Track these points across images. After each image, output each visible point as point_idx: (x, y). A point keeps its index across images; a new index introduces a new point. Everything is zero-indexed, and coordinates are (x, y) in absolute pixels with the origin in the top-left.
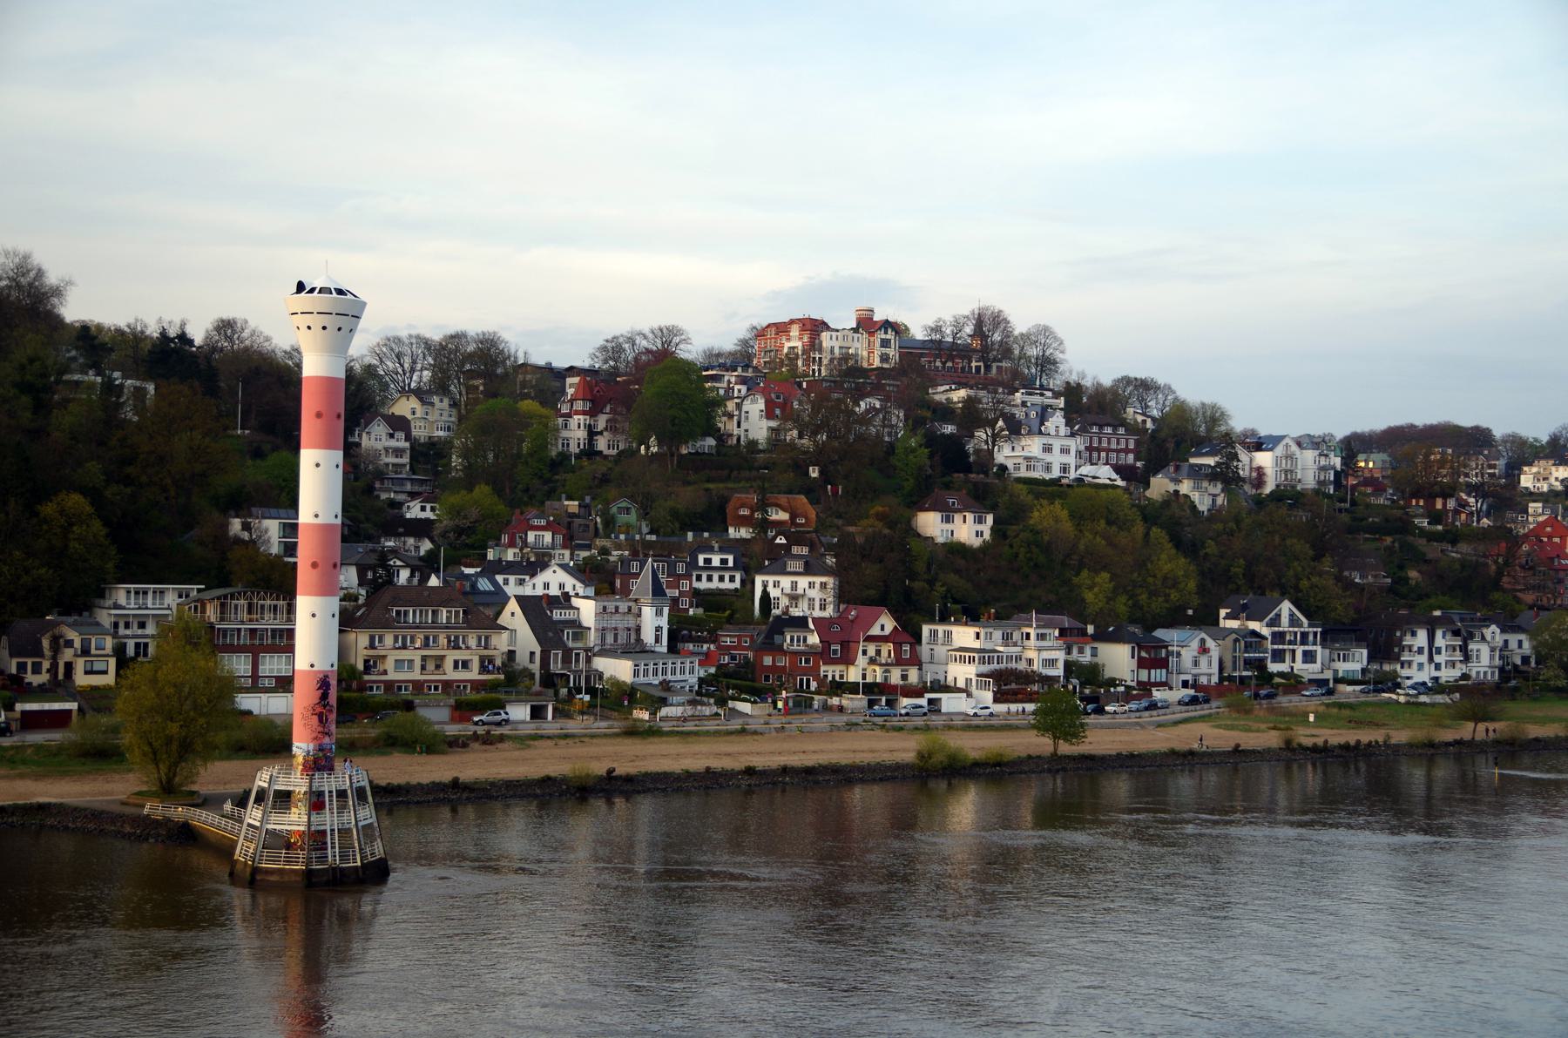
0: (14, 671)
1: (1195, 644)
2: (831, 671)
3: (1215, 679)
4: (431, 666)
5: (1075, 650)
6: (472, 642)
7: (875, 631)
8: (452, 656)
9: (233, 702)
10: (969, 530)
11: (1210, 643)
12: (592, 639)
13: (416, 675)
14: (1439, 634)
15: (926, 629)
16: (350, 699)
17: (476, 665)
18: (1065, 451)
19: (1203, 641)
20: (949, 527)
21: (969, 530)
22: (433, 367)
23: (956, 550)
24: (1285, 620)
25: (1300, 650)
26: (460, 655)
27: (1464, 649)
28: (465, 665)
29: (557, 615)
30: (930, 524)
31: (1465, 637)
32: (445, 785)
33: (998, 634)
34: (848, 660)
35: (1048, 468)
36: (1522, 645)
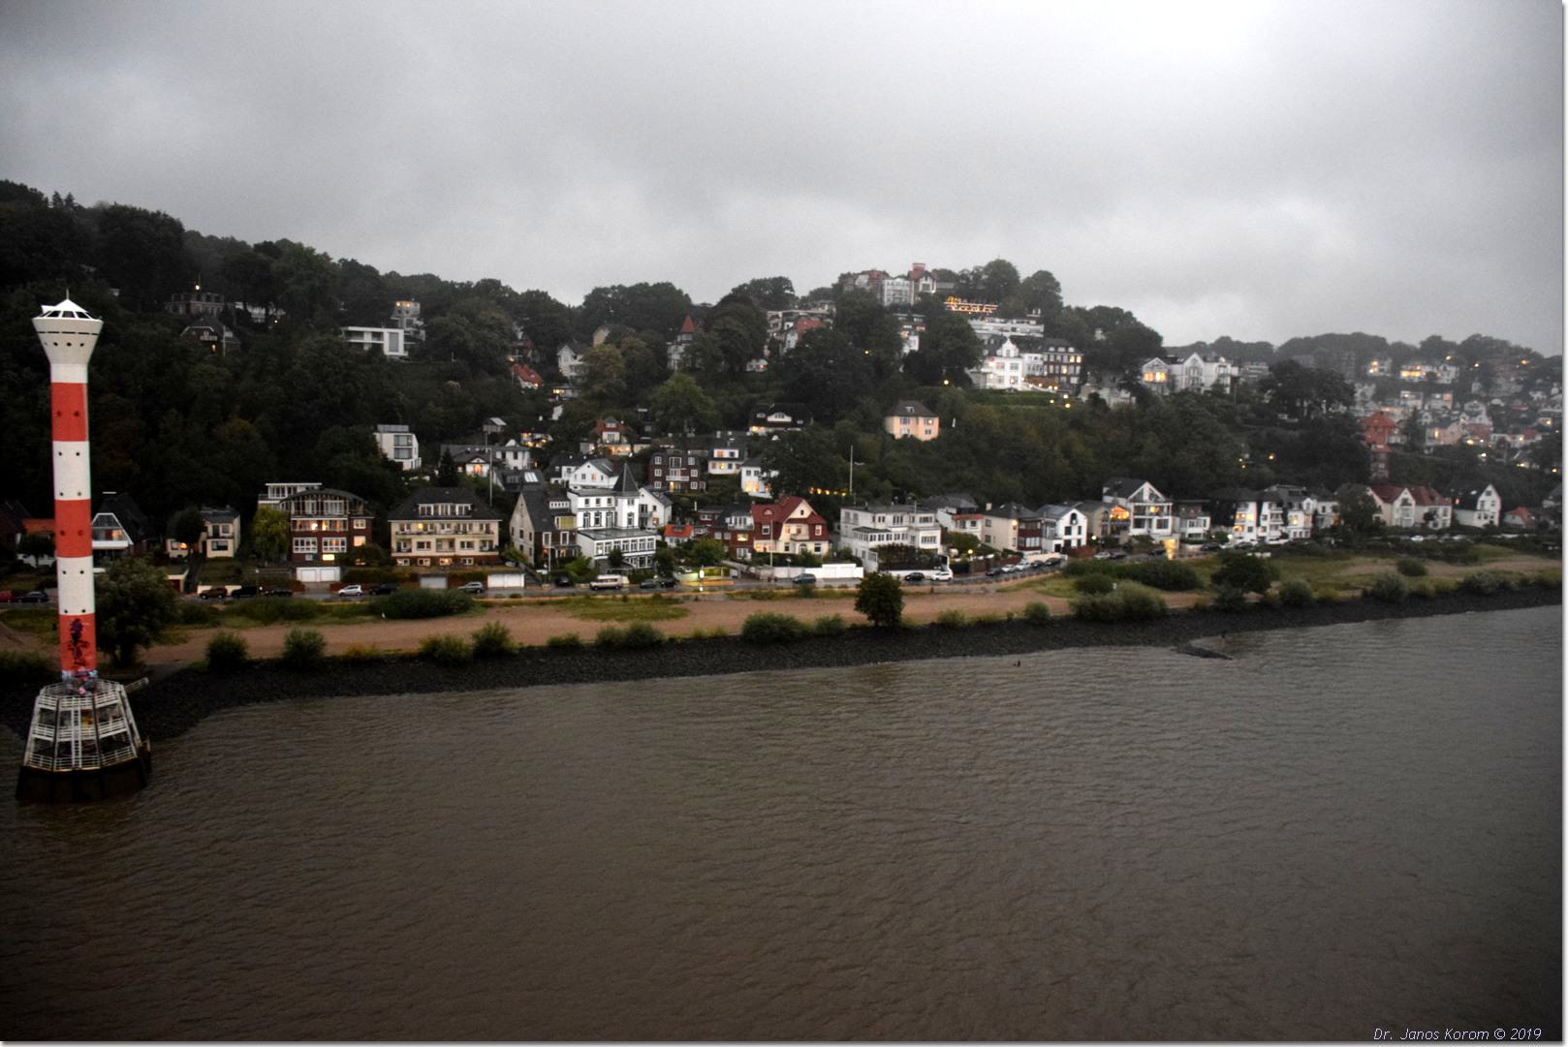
1: (1066, 518)
2: (759, 546)
3: (1084, 543)
4: (446, 546)
5: (968, 524)
6: (476, 528)
7: (796, 514)
8: (459, 539)
9: (294, 571)
10: (926, 429)
11: (1081, 517)
12: (579, 523)
13: (433, 552)
14: (1265, 506)
15: (843, 512)
16: (127, 614)
17: (477, 544)
18: (1014, 367)
19: (1074, 516)
21: (926, 429)
23: (909, 441)
24: (1146, 497)
25: (1155, 519)
26: (465, 539)
27: (1285, 517)
28: (421, 545)
29: (554, 505)
30: (898, 427)
31: (1284, 507)
35: (1001, 380)
36: (1328, 511)
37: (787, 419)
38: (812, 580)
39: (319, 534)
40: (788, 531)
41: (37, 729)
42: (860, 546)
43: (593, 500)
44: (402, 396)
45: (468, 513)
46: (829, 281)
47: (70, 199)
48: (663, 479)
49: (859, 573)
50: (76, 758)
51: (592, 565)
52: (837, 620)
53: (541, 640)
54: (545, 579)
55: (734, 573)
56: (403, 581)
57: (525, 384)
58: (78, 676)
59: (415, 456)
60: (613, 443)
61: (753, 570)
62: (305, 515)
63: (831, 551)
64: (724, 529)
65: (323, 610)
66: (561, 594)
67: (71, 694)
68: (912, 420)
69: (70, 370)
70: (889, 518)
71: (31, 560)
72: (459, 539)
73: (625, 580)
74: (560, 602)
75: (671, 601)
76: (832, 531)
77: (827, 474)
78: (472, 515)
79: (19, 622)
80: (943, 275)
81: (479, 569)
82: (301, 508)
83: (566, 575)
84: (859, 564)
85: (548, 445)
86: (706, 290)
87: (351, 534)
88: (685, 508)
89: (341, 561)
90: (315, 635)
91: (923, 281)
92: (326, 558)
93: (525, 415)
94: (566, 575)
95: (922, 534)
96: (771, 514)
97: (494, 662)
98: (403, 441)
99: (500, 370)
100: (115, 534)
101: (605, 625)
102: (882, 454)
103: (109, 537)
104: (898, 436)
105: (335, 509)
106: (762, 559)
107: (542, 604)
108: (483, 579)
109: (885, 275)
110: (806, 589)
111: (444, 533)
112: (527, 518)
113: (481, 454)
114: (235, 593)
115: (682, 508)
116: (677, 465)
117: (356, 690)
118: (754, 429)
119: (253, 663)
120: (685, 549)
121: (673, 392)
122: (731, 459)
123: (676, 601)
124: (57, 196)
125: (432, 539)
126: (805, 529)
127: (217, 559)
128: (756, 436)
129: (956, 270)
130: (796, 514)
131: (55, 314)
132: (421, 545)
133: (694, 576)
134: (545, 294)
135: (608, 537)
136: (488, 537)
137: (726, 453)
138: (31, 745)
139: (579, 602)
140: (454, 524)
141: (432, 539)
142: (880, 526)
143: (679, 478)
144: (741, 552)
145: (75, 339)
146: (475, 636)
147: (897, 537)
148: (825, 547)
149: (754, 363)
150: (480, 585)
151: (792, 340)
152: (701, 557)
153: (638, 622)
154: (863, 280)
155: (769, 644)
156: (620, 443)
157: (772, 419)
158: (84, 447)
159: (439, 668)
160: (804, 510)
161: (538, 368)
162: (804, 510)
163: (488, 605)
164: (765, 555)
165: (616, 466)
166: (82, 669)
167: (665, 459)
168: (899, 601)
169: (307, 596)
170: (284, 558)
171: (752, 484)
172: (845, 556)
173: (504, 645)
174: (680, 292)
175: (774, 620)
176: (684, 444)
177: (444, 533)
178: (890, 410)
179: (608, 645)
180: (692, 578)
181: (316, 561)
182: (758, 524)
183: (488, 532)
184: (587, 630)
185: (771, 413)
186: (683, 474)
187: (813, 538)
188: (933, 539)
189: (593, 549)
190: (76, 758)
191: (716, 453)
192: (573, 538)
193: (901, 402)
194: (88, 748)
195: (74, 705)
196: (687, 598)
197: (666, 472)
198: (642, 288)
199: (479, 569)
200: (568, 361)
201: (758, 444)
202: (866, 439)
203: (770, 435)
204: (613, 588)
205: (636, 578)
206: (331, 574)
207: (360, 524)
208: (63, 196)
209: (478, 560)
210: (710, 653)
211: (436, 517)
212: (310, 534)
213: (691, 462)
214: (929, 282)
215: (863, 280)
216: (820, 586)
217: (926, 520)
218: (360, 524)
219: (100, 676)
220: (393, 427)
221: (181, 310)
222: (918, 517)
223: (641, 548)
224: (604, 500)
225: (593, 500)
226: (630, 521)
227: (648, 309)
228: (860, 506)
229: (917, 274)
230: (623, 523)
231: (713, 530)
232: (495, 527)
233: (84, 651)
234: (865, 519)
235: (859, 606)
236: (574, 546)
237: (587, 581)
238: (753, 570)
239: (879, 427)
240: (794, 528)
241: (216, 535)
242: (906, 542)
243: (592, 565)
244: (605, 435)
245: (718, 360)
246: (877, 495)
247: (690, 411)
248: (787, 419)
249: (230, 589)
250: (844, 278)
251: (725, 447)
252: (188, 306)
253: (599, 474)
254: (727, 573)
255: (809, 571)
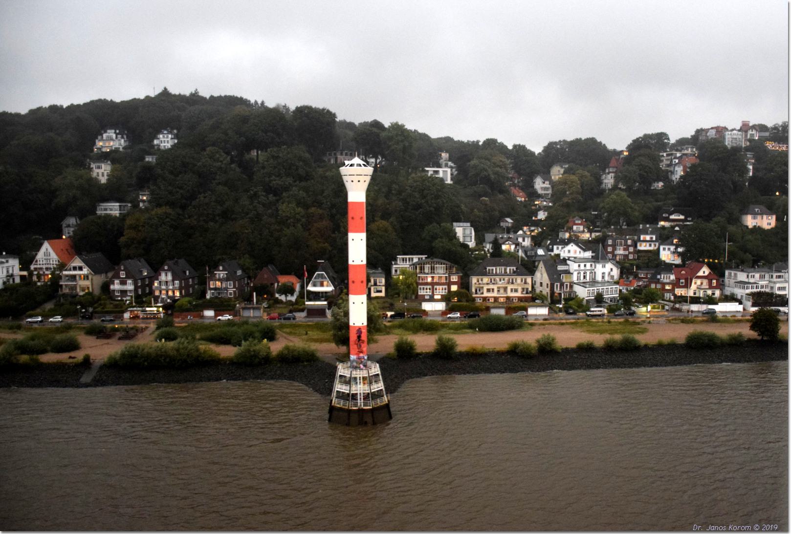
0: (129, 281)
2: (679, 292)
4: (502, 291)
6: (519, 281)
7: (700, 274)
8: (510, 287)
9: (421, 304)
12: (575, 278)
13: (495, 294)
15: (727, 272)
17: (520, 290)
20: (756, 221)
22: (266, 266)
23: (757, 230)
28: (488, 290)
29: (560, 268)
30: (750, 221)
32: (572, 349)
33: (757, 275)
34: (687, 286)
37: (682, 217)
38: (713, 312)
39: (433, 284)
40: (695, 284)
41: (339, 386)
42: (739, 292)
43: (582, 265)
44: (463, 207)
45: (514, 272)
46: (689, 133)
47: (263, 103)
48: (613, 253)
49: (740, 308)
50: (360, 402)
51: (584, 302)
52: (740, 335)
53: (573, 345)
54: (560, 310)
55: (667, 307)
56: (482, 310)
57: (519, 199)
58: (359, 358)
59: (473, 240)
60: (579, 232)
61: (677, 306)
62: (425, 273)
63: (722, 294)
64: (658, 281)
65: (443, 326)
66: (571, 318)
67: (356, 368)
68: (759, 217)
69: (357, 194)
70: (757, 275)
71: (283, 298)
72: (510, 287)
73: (606, 311)
74: (572, 323)
75: (635, 323)
76: (721, 286)
77: (718, 247)
78: (516, 273)
79: (288, 330)
80: (762, 128)
81: (522, 304)
82: (422, 269)
83: (571, 308)
84: (741, 303)
85: (539, 234)
86: (618, 140)
87: (449, 284)
88: (628, 270)
89: (446, 299)
90: (452, 340)
91: (750, 132)
92: (436, 297)
93: (525, 218)
94: (571, 308)
95: (778, 285)
96: (685, 271)
97: (546, 356)
98: (468, 232)
99: (503, 191)
100: (325, 283)
101: (607, 336)
102: (743, 237)
103: (322, 285)
104: (750, 227)
105: (441, 270)
106: (683, 299)
107: (562, 324)
108: (526, 310)
109: (726, 129)
110: (712, 317)
111: (501, 284)
112: (545, 276)
113: (509, 239)
114: (391, 316)
115: (626, 270)
116: (621, 245)
117: (476, 371)
118: (662, 223)
119: (418, 354)
120: (637, 292)
121: (615, 202)
122: (651, 241)
123: (638, 324)
124: (256, 102)
125: (495, 287)
126: (705, 282)
127: (377, 298)
128: (663, 227)
129: (770, 124)
130: (700, 274)
131: (351, 165)
132: (488, 290)
133: (644, 309)
134: (524, 147)
135: (592, 286)
136: (526, 286)
137: (648, 238)
138: (334, 394)
139: (583, 323)
140: (506, 278)
141: (495, 288)
142: (752, 280)
143: (622, 252)
144: (667, 296)
145: (362, 178)
146: (538, 341)
147: (762, 287)
148: (718, 293)
149: (656, 184)
150: (525, 313)
151: (679, 172)
152: (649, 298)
153: (626, 335)
154: (713, 132)
155: (701, 349)
156: (583, 231)
157: (672, 217)
158: (363, 236)
159: (518, 359)
160: (705, 271)
161: (522, 189)
162: (705, 271)
163: (532, 325)
164: (681, 297)
165: (586, 245)
166: (361, 355)
167: (614, 241)
168: (777, 324)
169: (429, 318)
170: (413, 297)
171: (667, 255)
172: (732, 298)
173: (553, 347)
174: (600, 143)
175: (705, 335)
176: (621, 233)
177: (501, 284)
178: (745, 211)
179: (609, 348)
180: (644, 311)
181: (432, 299)
182: (678, 279)
183: (525, 283)
184: (598, 340)
185: (671, 214)
186: (625, 249)
187: (711, 287)
188: (784, 288)
189: (582, 293)
190: (360, 402)
191: (642, 237)
192: (571, 287)
193: (751, 206)
194: (366, 397)
195: (360, 374)
196: (644, 321)
197: (614, 249)
198: (578, 142)
199: (522, 304)
200: (540, 184)
201: (666, 232)
202: (732, 228)
203: (673, 227)
204: (599, 315)
205: (611, 310)
206: (441, 306)
207: (454, 278)
208: (259, 102)
209: (520, 299)
210: (666, 354)
211: (496, 275)
212: (427, 284)
213: (629, 242)
214: (754, 132)
215: (712, 134)
216: (720, 316)
217: (779, 277)
218: (454, 278)
219: (369, 359)
220: (461, 224)
221: (332, 161)
222: (775, 275)
223: (611, 293)
224: (588, 265)
225: (582, 265)
226: (603, 277)
227: (584, 154)
228: (737, 268)
229: (745, 128)
230: (599, 278)
231: (650, 283)
232: (529, 280)
233: (363, 345)
234: (742, 276)
235: (752, 328)
236: (572, 291)
237: (584, 311)
238: (677, 306)
239: (736, 220)
240: (699, 282)
241: (375, 284)
242: (768, 290)
243: (584, 302)
244: (575, 228)
245: (635, 182)
246: (742, 262)
247: (625, 214)
248: (682, 217)
249: (389, 314)
250: (699, 132)
251: (647, 233)
252: (336, 159)
253: (578, 249)
254: (663, 308)
255: (711, 307)
